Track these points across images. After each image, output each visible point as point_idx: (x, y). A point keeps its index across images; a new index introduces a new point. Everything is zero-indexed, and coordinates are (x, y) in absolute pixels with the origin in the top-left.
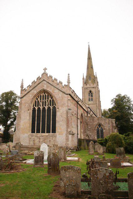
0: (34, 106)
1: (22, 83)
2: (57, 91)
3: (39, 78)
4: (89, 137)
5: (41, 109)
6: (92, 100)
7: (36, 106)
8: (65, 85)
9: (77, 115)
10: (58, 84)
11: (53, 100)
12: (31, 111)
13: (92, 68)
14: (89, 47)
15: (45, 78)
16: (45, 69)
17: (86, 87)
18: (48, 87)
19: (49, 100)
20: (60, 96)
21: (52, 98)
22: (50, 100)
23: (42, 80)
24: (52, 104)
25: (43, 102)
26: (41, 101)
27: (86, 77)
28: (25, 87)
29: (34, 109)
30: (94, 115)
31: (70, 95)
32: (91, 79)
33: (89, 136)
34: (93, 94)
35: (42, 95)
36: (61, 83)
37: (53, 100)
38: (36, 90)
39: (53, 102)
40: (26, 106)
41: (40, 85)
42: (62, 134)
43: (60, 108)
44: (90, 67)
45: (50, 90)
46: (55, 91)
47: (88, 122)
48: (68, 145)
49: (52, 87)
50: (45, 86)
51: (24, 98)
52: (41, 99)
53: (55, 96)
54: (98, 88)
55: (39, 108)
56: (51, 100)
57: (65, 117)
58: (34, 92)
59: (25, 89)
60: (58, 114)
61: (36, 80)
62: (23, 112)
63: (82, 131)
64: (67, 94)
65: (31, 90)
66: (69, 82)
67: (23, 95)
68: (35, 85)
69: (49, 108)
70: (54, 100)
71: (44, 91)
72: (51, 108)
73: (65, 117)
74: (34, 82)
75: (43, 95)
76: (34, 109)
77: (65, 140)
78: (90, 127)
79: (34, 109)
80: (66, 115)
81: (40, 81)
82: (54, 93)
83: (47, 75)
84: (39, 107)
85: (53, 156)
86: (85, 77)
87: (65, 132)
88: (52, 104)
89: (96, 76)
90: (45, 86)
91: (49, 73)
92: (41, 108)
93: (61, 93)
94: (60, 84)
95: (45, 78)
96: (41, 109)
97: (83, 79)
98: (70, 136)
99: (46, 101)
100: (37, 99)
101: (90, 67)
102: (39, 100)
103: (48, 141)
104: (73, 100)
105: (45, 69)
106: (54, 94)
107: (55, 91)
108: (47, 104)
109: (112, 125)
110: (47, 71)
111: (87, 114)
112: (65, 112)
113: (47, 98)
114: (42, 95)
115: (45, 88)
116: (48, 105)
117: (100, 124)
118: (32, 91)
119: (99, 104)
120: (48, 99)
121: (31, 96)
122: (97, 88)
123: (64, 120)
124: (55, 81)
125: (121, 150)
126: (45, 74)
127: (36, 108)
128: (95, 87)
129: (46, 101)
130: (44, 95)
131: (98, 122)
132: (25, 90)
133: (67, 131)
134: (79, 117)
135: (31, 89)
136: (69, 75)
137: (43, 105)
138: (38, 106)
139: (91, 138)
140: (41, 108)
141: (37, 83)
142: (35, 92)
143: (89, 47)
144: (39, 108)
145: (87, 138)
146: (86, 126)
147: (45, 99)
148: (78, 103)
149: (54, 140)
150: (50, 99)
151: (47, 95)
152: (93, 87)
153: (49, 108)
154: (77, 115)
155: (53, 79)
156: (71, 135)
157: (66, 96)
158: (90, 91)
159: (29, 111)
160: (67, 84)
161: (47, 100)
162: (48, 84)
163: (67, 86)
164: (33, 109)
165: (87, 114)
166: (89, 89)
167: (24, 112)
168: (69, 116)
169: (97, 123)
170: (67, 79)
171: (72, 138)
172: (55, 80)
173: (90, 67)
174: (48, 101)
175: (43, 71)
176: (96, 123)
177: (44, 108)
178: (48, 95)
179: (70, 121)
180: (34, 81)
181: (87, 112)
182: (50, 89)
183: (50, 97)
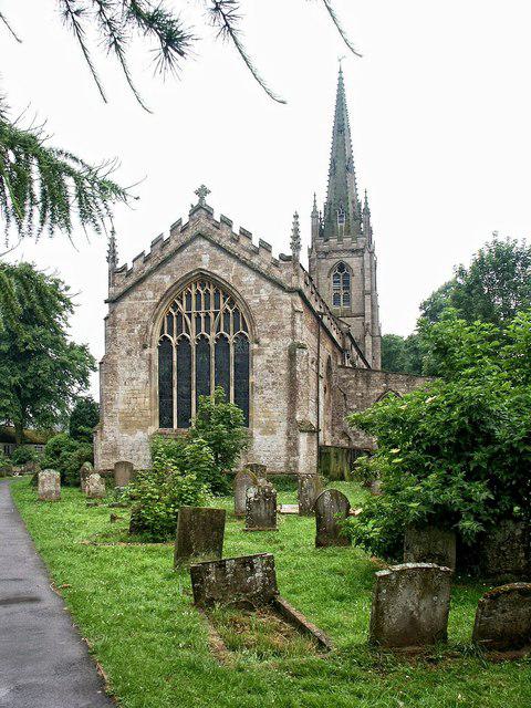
0: (162, 332)
2: (250, 278)
4: (350, 439)
5: (193, 344)
6: (347, 299)
9: (317, 364)
10: (255, 252)
12: (154, 351)
13: (349, 169)
14: (341, 79)
17: (326, 247)
18: (214, 261)
19: (221, 311)
20: (265, 296)
23: (189, 234)
24: (232, 325)
25: (198, 317)
26: (189, 315)
27: (328, 206)
28: (125, 258)
29: (165, 341)
31: (300, 293)
32: (342, 220)
33: (353, 438)
35: (193, 292)
36: (266, 247)
38: (169, 272)
39: (239, 317)
40: (132, 331)
41: (185, 253)
42: (273, 432)
43: (265, 340)
44: (341, 167)
45: (224, 276)
48: (296, 466)
49: (235, 265)
50: (206, 258)
51: (126, 302)
52: (189, 308)
55: (184, 341)
56: (231, 311)
57: (283, 372)
59: (124, 268)
61: (167, 235)
62: (123, 353)
63: (329, 418)
65: (150, 272)
68: (166, 253)
69: (222, 339)
70: (242, 310)
71: (204, 278)
72: (231, 338)
74: (159, 243)
76: (165, 345)
77: (283, 453)
78: (355, 406)
80: (285, 365)
81: (183, 239)
82: (240, 284)
83: (209, 213)
84: (184, 337)
85: (331, 498)
86: (321, 208)
87: (284, 424)
88: (232, 325)
89: (366, 203)
90: (206, 258)
92: (192, 337)
93: (268, 285)
94: (262, 252)
96: (193, 344)
98: (303, 439)
99: (212, 315)
100: (175, 306)
101: (340, 169)
105: (202, 192)
106: (240, 289)
107: (245, 280)
108: (213, 323)
110: (209, 200)
111: (343, 360)
112: (283, 356)
113: (212, 301)
114: (193, 292)
115: (204, 267)
116: (218, 330)
118: (156, 277)
119: (372, 317)
120: (217, 307)
122: (367, 255)
126: (201, 210)
127: (174, 340)
128: (362, 251)
129: (212, 315)
133: (291, 419)
134: (322, 372)
135: (148, 267)
136: (296, 217)
137: (198, 329)
139: (357, 444)
140: (192, 337)
141: (174, 245)
143: (341, 79)
144: (184, 341)
145: (343, 442)
146: (342, 401)
147: (207, 307)
148: (320, 321)
150: (224, 305)
151: (212, 291)
152: (353, 251)
153: (222, 339)
154: (317, 364)
155: (236, 230)
157: (286, 297)
158: (342, 267)
159: (146, 352)
160: (289, 253)
161: (212, 309)
162: (214, 250)
165: (343, 360)
166: (334, 255)
167: (129, 353)
168: (298, 369)
169: (381, 391)
172: (242, 237)
173: (341, 167)
174: (216, 314)
175: (195, 201)
177: (203, 340)
178: (217, 291)
180: (160, 238)
181: (342, 351)
182: (226, 271)
183: (224, 299)
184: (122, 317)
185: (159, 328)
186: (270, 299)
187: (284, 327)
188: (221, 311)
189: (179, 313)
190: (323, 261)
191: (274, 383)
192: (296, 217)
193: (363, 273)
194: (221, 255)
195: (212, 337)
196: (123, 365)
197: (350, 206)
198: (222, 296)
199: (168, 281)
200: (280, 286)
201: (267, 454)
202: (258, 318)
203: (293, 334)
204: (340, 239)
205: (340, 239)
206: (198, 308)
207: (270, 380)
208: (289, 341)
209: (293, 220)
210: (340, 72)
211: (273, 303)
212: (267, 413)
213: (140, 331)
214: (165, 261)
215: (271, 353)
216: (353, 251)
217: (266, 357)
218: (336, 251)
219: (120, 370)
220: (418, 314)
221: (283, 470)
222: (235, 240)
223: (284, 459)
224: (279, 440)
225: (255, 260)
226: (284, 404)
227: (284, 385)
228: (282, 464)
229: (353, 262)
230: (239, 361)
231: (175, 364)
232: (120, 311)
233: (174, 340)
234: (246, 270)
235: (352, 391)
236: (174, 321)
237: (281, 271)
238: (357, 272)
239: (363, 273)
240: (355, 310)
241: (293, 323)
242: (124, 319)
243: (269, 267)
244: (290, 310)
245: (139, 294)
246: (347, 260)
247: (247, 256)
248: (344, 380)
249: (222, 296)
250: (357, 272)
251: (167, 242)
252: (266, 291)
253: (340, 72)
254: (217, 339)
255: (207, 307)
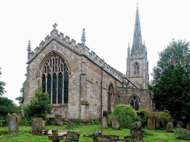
1: (29, 46)
2: (68, 52)
3: (48, 38)
6: (138, 72)
7: (45, 73)
8: (79, 44)
10: (70, 43)
11: (65, 64)
12: (41, 79)
13: (140, 35)
14: (137, 9)
15: (55, 37)
16: (55, 25)
18: (58, 48)
19: (60, 65)
20: (73, 58)
21: (63, 61)
22: (62, 64)
23: (50, 40)
26: (51, 66)
29: (44, 75)
30: (134, 87)
34: (140, 67)
35: (52, 59)
36: (74, 41)
37: (65, 64)
39: (65, 66)
41: (49, 46)
42: (75, 105)
43: (72, 73)
44: (137, 35)
45: (60, 52)
46: (67, 53)
47: (121, 94)
49: (63, 48)
50: (55, 47)
51: (33, 63)
52: (51, 64)
53: (67, 59)
54: (146, 59)
55: (49, 75)
56: (63, 64)
58: (42, 56)
60: (70, 81)
62: (31, 79)
64: (81, 56)
66: (83, 39)
67: (31, 59)
69: (60, 74)
70: (66, 63)
71: (55, 54)
72: (63, 73)
73: (78, 84)
74: (42, 43)
75: (54, 58)
77: (78, 112)
78: (122, 100)
79: (44, 75)
80: (79, 82)
82: (65, 54)
83: (57, 31)
86: (131, 48)
88: (63, 69)
89: (144, 44)
90: (55, 47)
91: (59, 29)
93: (74, 54)
94: (73, 43)
95: (55, 37)
97: (129, 49)
98: (83, 107)
100: (47, 64)
101: (137, 35)
102: (49, 64)
103: (59, 112)
104: (92, 64)
105: (55, 25)
106: (65, 56)
107: (67, 53)
108: (58, 68)
109: (150, 97)
112: (78, 78)
114: (52, 59)
115: (55, 50)
116: (59, 71)
117: (134, 96)
118: (41, 54)
120: (59, 63)
121: (39, 60)
122: (144, 60)
123: (77, 88)
124: (67, 40)
125: (137, 124)
126: (55, 31)
129: (57, 66)
130: (55, 58)
131: (133, 94)
132: (32, 54)
135: (39, 51)
138: (48, 72)
140: (51, 73)
141: (46, 43)
142: (43, 55)
143: (137, 9)
144: (49, 75)
146: (118, 98)
147: (56, 64)
149: (66, 112)
151: (57, 58)
152: (140, 59)
153: (60, 74)
155: (90, 51)
156: (84, 106)
157: (80, 58)
158: (136, 63)
159: (38, 79)
160: (81, 42)
161: (58, 64)
162: (58, 44)
163: (82, 45)
164: (42, 75)
166: (134, 60)
167: (33, 79)
168: (82, 83)
169: (131, 95)
170: (82, 36)
171: (86, 108)
173: (137, 35)
174: (59, 65)
175: (52, 28)
176: (130, 95)
179: (83, 89)
180: (42, 42)
182: (61, 51)
183: (61, 60)
184: (31, 68)
185: (42, 71)
186: (75, 59)
187: (79, 68)
188: (60, 65)
189: (48, 66)
190: (131, 62)
191: (75, 88)
192: (84, 30)
193: (143, 65)
194: (60, 45)
195: (57, 73)
196: (31, 83)
197: (140, 45)
198: (60, 59)
199: (44, 55)
200: (77, 54)
201: (73, 112)
202: (71, 65)
203: (82, 70)
204: (136, 55)
205: (136, 55)
206: (54, 64)
207: (74, 87)
208: (80, 73)
209: (83, 31)
210: (137, 7)
211: (76, 60)
212: (73, 99)
213: (36, 72)
214: (43, 49)
215: (74, 77)
216: (140, 59)
217: (73, 79)
218: (135, 59)
219: (30, 85)
220: (86, 39)
221: (78, 118)
222: (64, 40)
223: (78, 114)
224: (77, 108)
225: (70, 46)
226: (78, 95)
227: (79, 88)
228: (77, 116)
229: (140, 62)
230: (65, 81)
231: (46, 83)
232: (31, 66)
233: (46, 75)
234: (67, 50)
235: (121, 95)
236: (47, 69)
237: (78, 49)
238: (141, 65)
239: (143, 65)
240: (140, 76)
241: (82, 66)
242: (31, 69)
243: (74, 48)
244: (81, 62)
245: (36, 60)
246: (138, 61)
247: (68, 45)
248: (119, 91)
249: (60, 59)
250: (141, 65)
251: (44, 43)
252: (73, 56)
253: (137, 7)
254: (59, 74)
255: (56, 64)
